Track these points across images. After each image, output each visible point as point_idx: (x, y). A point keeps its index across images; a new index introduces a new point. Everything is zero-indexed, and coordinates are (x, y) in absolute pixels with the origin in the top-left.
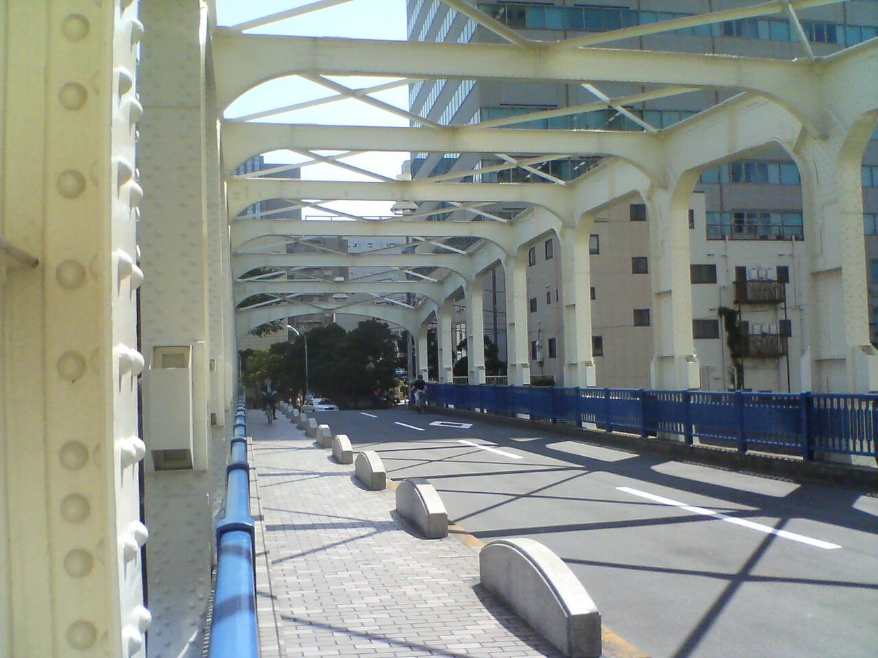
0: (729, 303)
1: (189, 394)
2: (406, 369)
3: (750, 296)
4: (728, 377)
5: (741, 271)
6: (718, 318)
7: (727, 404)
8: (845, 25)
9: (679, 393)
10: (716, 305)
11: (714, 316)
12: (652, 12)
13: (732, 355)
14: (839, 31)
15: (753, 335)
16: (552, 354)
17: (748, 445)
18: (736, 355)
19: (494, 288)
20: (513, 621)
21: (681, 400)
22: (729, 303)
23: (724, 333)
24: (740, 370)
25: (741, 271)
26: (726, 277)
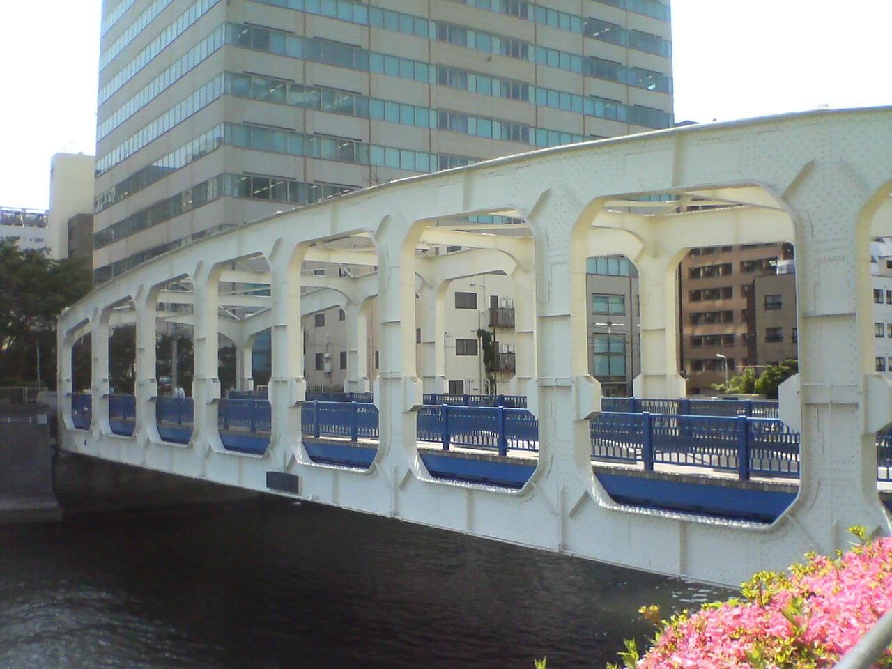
0: (485, 326)
1: (281, 497)
2: (170, 377)
3: (501, 322)
4: (483, 389)
5: (494, 300)
6: (477, 339)
7: (706, 437)
8: (536, 128)
9: (429, 395)
10: (476, 328)
11: (474, 336)
12: (381, 54)
13: (486, 369)
14: (532, 132)
15: (502, 354)
16: (343, 365)
17: (751, 473)
18: (490, 370)
19: (631, 330)
20: (108, 611)
21: (678, 434)
22: (485, 326)
23: (481, 351)
24: (493, 382)
25: (494, 300)
26: (483, 304)
